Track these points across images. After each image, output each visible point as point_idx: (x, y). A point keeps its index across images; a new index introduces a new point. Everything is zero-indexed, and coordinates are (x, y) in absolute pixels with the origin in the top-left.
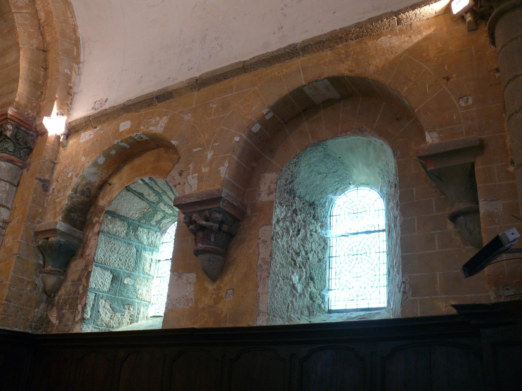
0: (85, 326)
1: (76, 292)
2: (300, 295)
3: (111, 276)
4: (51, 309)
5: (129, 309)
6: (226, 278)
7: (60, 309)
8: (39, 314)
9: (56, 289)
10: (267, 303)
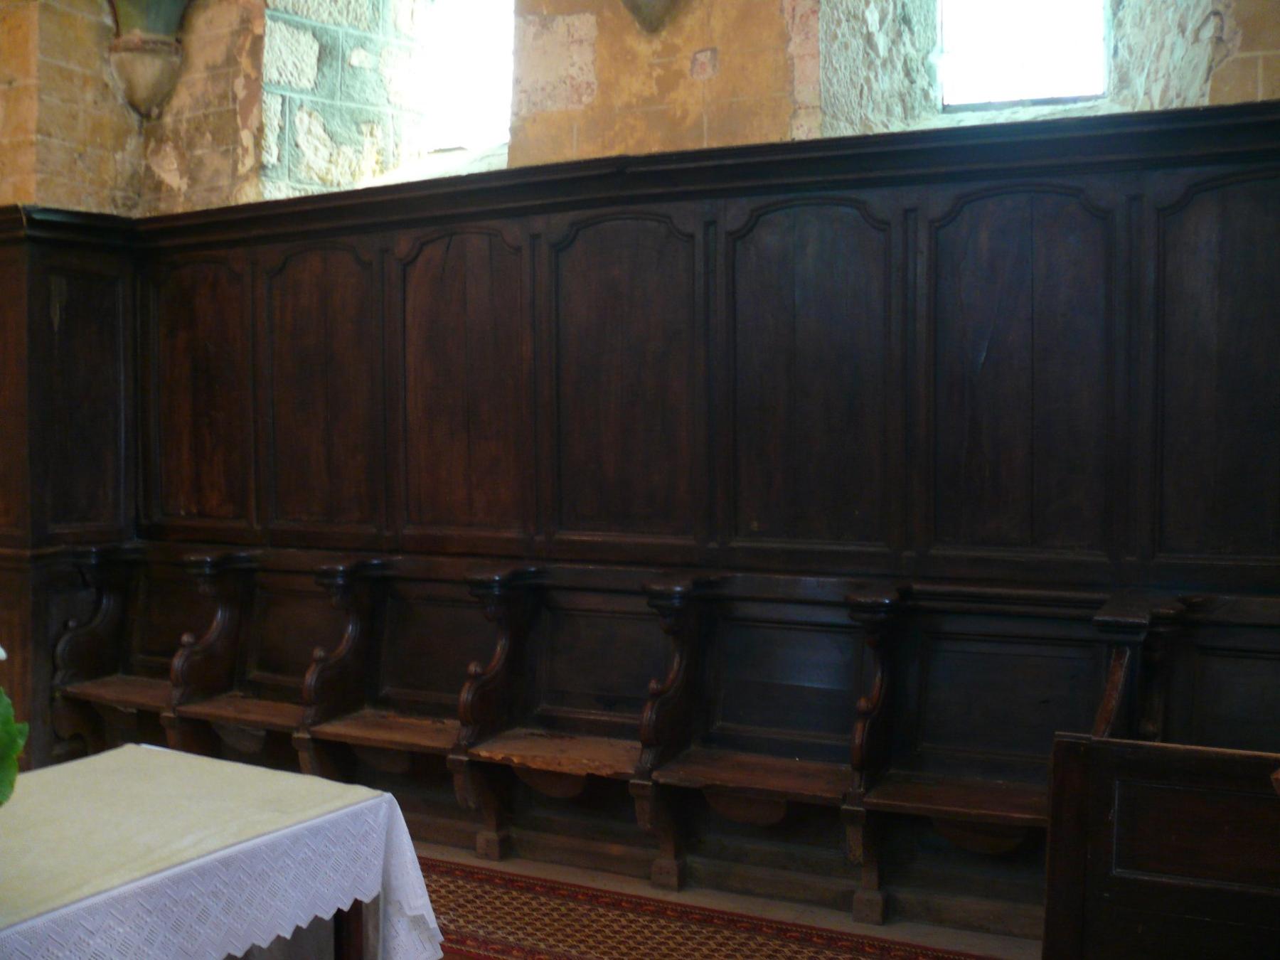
0: (269, 185)
1: (227, 96)
2: (884, 65)
3: (316, 47)
4: (156, 151)
5: (371, 134)
6: (690, 22)
7: (185, 148)
8: (128, 167)
9: (163, 95)
10: (818, 81)
